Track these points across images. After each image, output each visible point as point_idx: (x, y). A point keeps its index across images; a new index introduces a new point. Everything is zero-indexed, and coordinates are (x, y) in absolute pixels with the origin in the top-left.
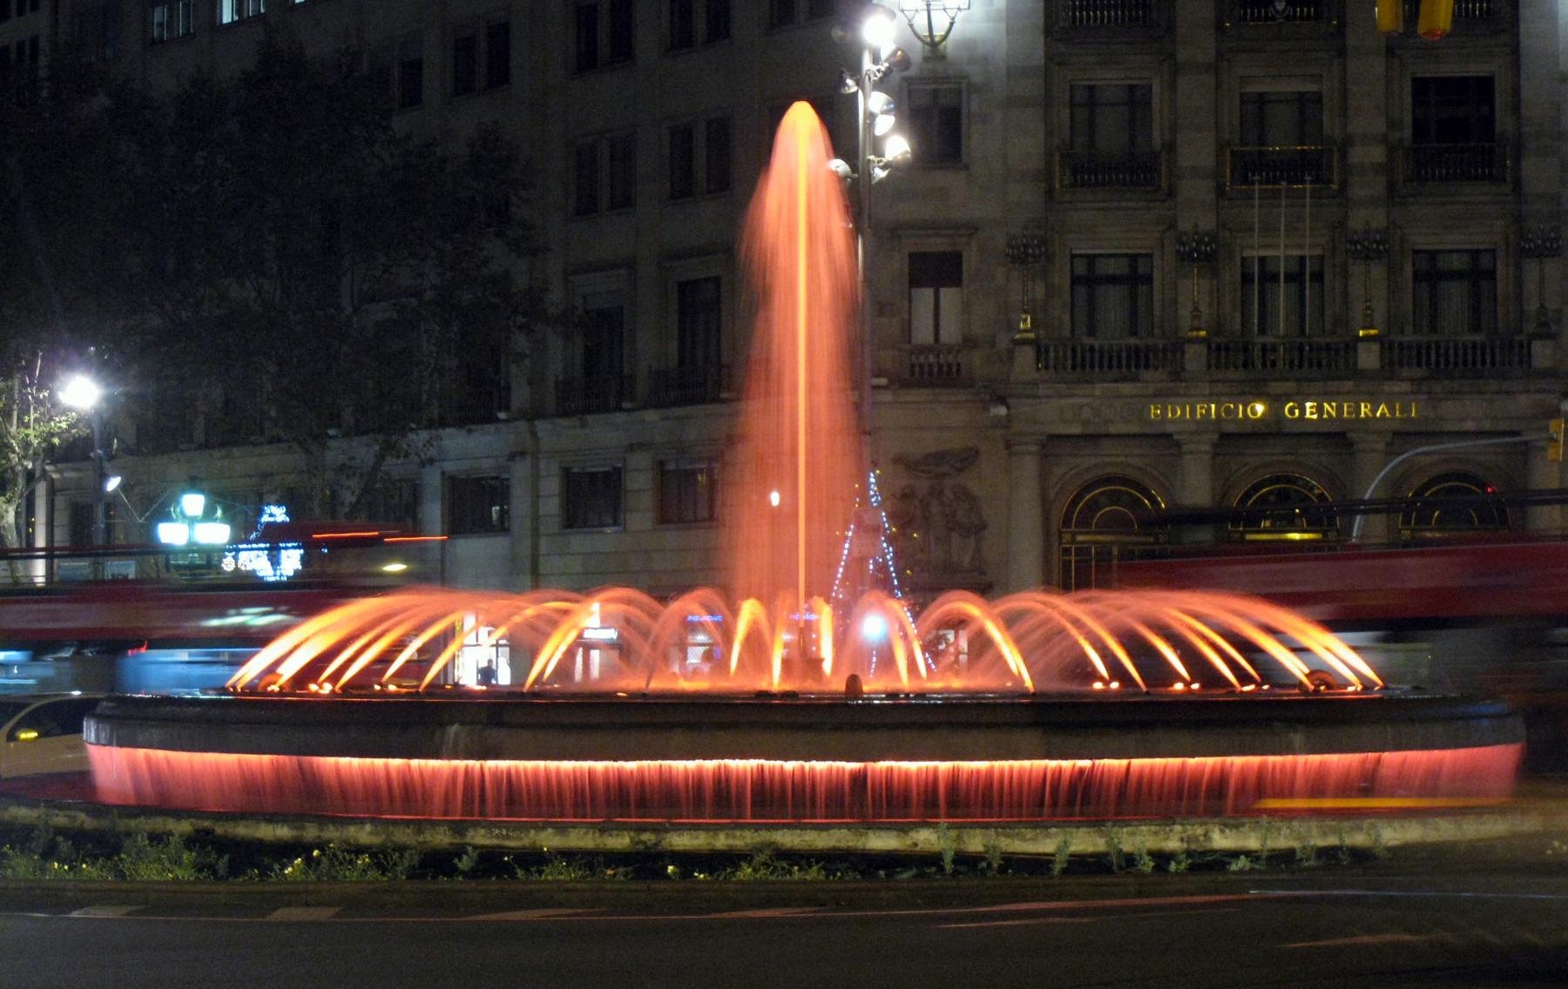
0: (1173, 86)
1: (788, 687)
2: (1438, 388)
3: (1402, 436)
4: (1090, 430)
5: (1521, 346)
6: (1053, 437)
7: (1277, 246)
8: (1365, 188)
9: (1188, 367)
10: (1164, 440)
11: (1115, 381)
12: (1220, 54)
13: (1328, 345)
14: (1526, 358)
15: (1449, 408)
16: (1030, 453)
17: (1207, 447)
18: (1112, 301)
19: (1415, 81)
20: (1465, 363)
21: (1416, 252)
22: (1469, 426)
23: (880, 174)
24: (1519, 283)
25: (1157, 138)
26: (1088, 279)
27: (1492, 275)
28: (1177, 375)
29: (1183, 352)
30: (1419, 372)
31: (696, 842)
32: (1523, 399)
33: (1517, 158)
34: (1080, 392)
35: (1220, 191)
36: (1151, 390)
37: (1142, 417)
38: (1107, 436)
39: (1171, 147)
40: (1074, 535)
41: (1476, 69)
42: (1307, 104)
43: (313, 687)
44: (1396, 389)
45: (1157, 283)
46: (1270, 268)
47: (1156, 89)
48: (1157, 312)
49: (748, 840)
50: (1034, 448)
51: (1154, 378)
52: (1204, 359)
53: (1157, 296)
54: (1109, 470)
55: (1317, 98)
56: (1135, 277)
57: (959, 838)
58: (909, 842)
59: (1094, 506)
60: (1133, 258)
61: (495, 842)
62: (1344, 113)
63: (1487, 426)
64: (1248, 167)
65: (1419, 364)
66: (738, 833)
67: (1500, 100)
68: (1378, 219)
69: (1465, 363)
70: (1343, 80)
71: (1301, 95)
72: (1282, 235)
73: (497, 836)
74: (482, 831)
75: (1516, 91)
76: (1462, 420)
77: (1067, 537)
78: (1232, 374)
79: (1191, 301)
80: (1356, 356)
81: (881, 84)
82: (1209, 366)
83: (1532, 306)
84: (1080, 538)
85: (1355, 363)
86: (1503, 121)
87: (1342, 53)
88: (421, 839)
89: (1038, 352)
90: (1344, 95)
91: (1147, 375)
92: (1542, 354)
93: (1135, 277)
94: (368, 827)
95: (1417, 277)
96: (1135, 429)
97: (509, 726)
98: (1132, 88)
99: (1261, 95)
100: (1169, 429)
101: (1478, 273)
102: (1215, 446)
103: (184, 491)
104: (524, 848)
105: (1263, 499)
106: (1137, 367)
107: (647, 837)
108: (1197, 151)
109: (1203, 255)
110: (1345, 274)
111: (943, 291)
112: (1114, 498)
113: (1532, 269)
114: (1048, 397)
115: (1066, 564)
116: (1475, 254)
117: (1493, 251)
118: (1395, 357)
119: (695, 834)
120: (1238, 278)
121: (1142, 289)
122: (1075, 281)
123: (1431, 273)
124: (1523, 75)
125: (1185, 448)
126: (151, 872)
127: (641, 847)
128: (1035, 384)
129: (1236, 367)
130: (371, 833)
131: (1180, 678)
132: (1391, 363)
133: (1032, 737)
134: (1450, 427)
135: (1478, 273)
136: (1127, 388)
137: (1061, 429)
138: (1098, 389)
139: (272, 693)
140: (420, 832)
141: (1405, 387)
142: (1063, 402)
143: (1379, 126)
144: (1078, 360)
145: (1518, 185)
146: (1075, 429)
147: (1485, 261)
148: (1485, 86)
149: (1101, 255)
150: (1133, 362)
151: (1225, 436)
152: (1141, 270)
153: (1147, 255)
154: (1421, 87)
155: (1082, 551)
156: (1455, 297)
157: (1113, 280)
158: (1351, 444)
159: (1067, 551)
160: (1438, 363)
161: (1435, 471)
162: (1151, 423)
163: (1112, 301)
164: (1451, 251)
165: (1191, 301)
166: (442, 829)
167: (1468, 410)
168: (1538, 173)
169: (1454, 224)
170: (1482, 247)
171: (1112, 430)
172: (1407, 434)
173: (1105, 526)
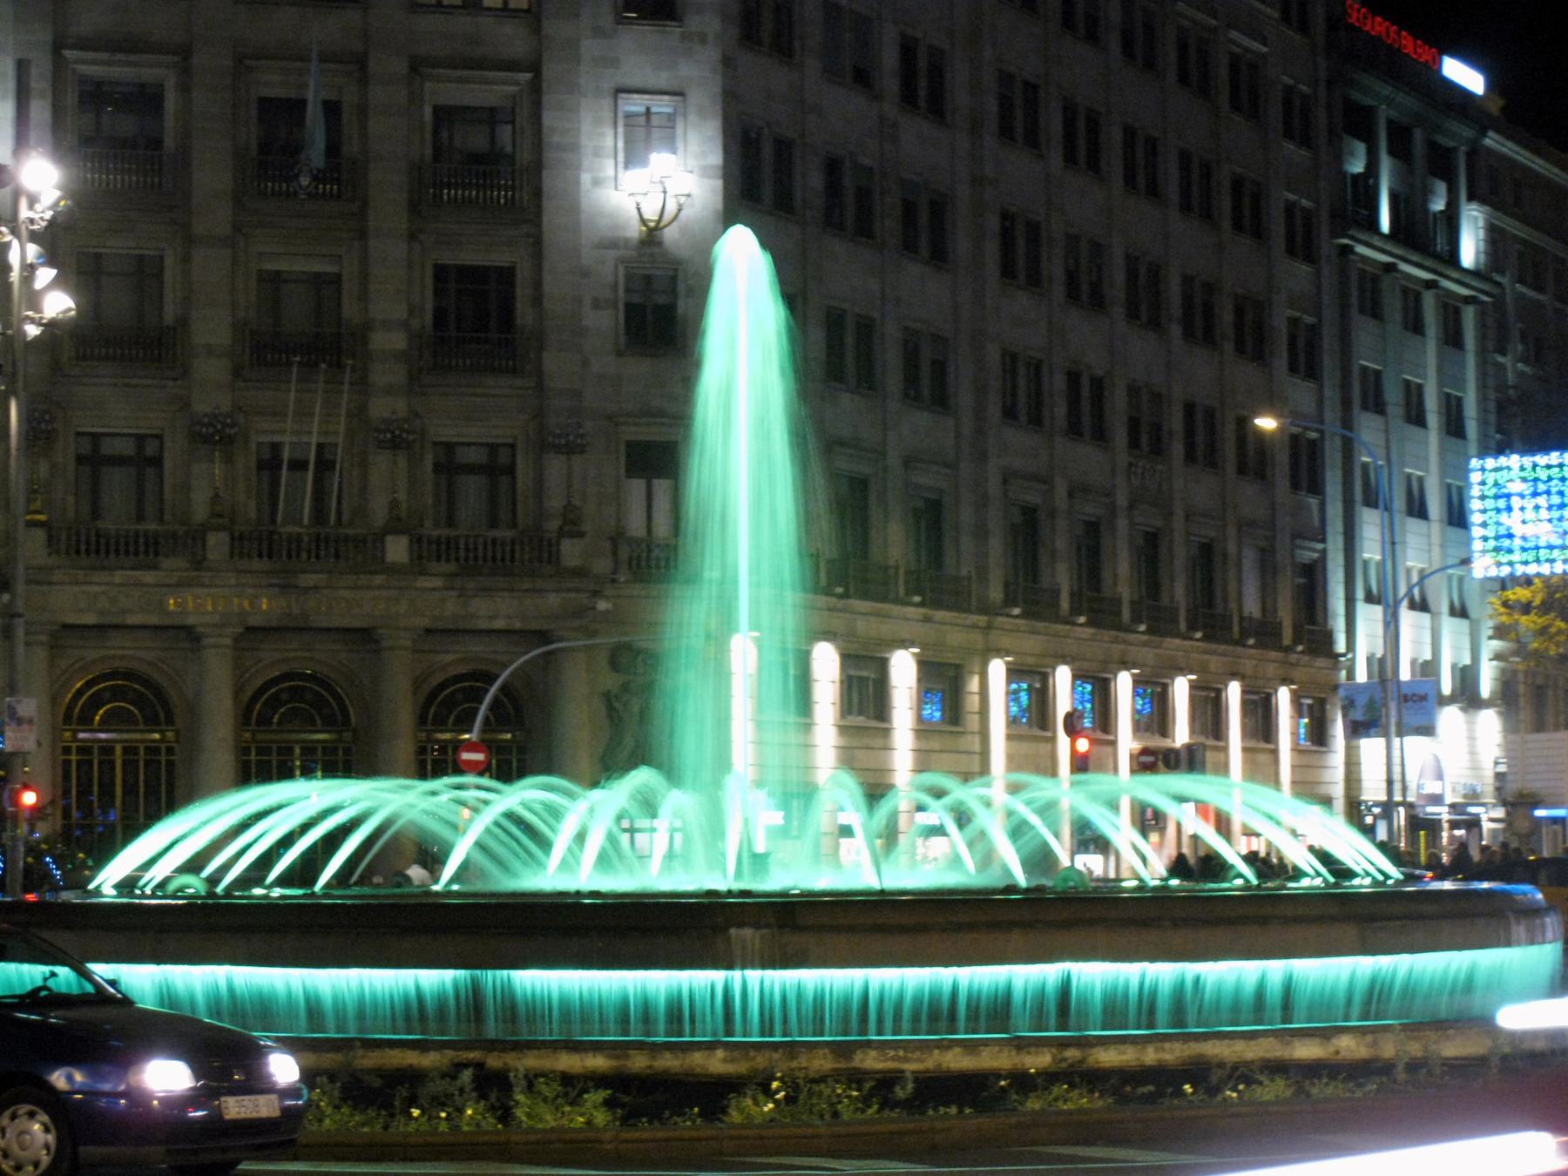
0: (186, 259)
1: (1034, 883)
2: (471, 585)
3: (253, 634)
4: (107, 620)
5: (550, 545)
6: (65, 626)
7: (283, 432)
8: (386, 374)
9: (210, 556)
10: (187, 636)
11: (133, 568)
12: (237, 228)
13: (439, 537)
14: (554, 557)
15: (480, 606)
16: (42, 644)
17: (228, 641)
18: (117, 484)
19: (436, 266)
20: (494, 559)
21: (78, 434)
22: (500, 624)
23: (32, 331)
24: (539, 481)
25: (170, 313)
26: (93, 460)
27: (510, 470)
28: (199, 563)
29: (204, 541)
30: (452, 567)
31: (1125, 1057)
32: (553, 600)
33: (541, 349)
34: (96, 579)
35: (237, 372)
36: (174, 580)
37: (162, 605)
38: (127, 627)
39: (183, 322)
40: (75, 732)
41: (499, 258)
42: (325, 286)
43: (258, 891)
44: (428, 585)
45: (168, 464)
46: (328, 456)
47: (169, 261)
48: (167, 496)
49: (1178, 1053)
50: (44, 638)
51: (174, 565)
52: (226, 549)
53: (168, 480)
54: (117, 664)
55: (337, 280)
56: (145, 459)
57: (1375, 1044)
58: (1331, 1049)
59: (275, 702)
60: (140, 439)
61: (890, 1065)
62: (363, 296)
63: (518, 625)
64: (267, 350)
65: (448, 560)
66: (1167, 1045)
67: (522, 292)
68: (400, 406)
69: (494, 559)
70: (364, 260)
71: (317, 275)
72: (301, 419)
73: (893, 1059)
74: (873, 1053)
75: (538, 284)
76: (494, 618)
77: (170, 735)
78: (256, 564)
79: (202, 484)
80: (383, 551)
81: (34, 237)
82: (232, 555)
83: (555, 503)
84: (81, 735)
85: (383, 557)
86: (524, 314)
87: (363, 234)
88: (794, 1064)
89: (50, 538)
90: (364, 278)
91: (167, 563)
92: (571, 552)
93: (145, 459)
94: (720, 1053)
95: (438, 468)
96: (154, 620)
97: (803, 929)
98: (141, 258)
99: (278, 273)
100: (191, 621)
101: (497, 466)
102: (236, 640)
103: (838, 647)
104: (927, 1071)
105: (275, 697)
106: (157, 554)
107: (1072, 1054)
108: (212, 330)
109: (215, 437)
110: (364, 464)
111: (656, 482)
112: (118, 693)
113: (555, 467)
114: (63, 583)
115: (67, 763)
116: (493, 448)
117: (512, 446)
118: (427, 552)
119: (1122, 1047)
120: (253, 464)
121: (150, 472)
122: (80, 460)
123: (449, 466)
124: (546, 266)
125: (206, 641)
126: (535, 1115)
127: (1064, 1065)
128: (51, 569)
129: (260, 556)
130: (725, 1060)
131: (1307, 875)
132: (420, 557)
133: (1350, 932)
134: (483, 624)
135: (497, 466)
136: (149, 577)
137: (72, 619)
138: (118, 576)
139: (437, 894)
140: (792, 1057)
141: (438, 582)
142: (76, 589)
143: (401, 312)
144: (88, 545)
145: (539, 373)
146: (90, 619)
147: (503, 457)
148: (506, 275)
149: (108, 435)
150: (144, 549)
151: (250, 630)
152: (150, 449)
153: (156, 436)
154: (441, 272)
155: (85, 750)
156: (472, 489)
157: (120, 461)
158: (377, 641)
159: (67, 750)
160: (466, 559)
161: (462, 669)
162: (169, 614)
163: (472, 489)
164: (469, 444)
165: (202, 484)
166: (821, 1052)
167: (498, 609)
168: (555, 363)
169: (473, 415)
170: (500, 441)
171: (132, 620)
172: (286, 629)
173: (105, 725)
